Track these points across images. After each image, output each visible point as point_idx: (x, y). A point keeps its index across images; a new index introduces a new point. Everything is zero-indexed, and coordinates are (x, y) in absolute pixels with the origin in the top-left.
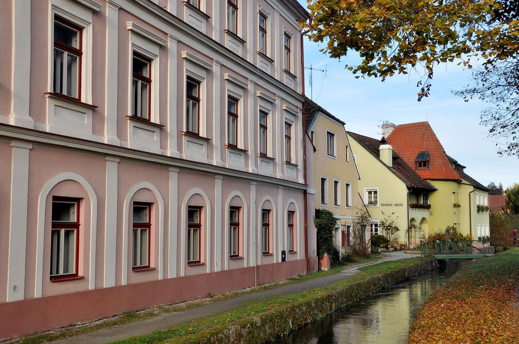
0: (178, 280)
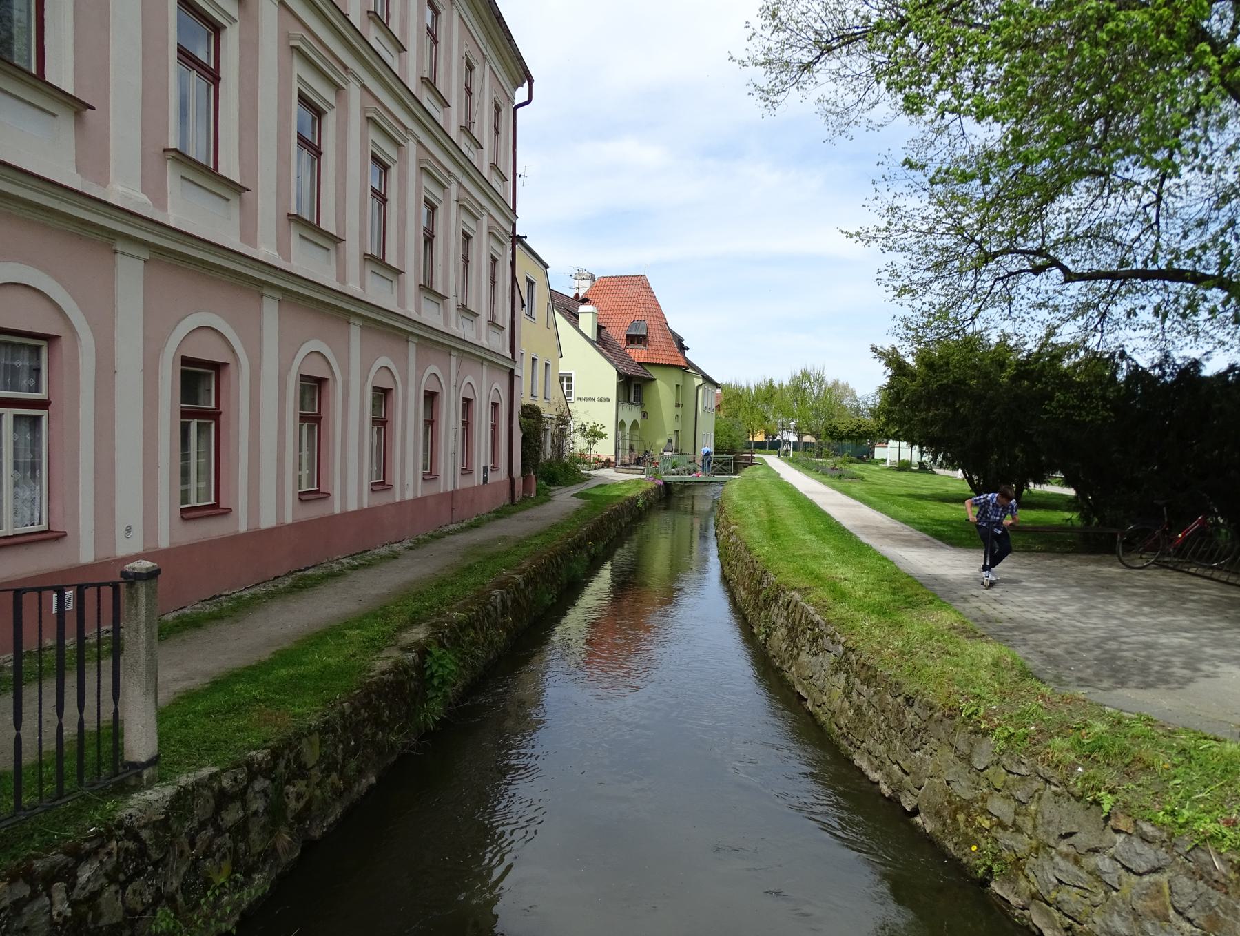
0: (361, 512)
